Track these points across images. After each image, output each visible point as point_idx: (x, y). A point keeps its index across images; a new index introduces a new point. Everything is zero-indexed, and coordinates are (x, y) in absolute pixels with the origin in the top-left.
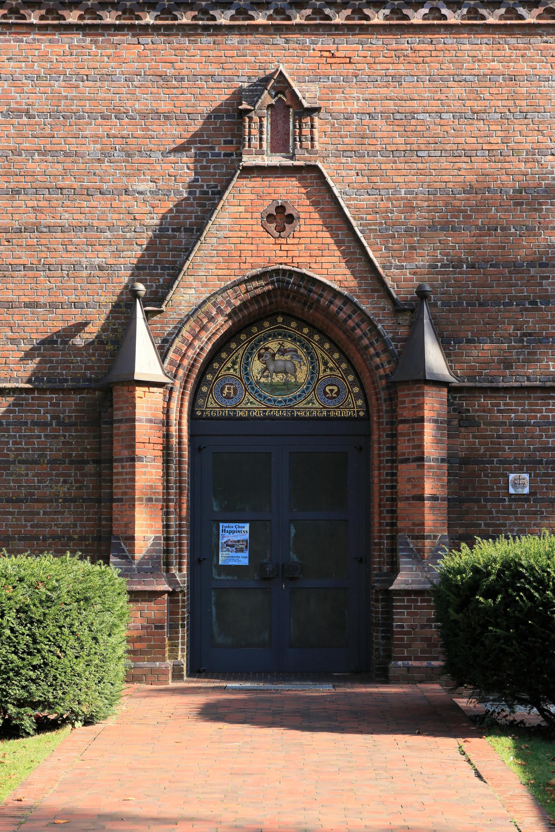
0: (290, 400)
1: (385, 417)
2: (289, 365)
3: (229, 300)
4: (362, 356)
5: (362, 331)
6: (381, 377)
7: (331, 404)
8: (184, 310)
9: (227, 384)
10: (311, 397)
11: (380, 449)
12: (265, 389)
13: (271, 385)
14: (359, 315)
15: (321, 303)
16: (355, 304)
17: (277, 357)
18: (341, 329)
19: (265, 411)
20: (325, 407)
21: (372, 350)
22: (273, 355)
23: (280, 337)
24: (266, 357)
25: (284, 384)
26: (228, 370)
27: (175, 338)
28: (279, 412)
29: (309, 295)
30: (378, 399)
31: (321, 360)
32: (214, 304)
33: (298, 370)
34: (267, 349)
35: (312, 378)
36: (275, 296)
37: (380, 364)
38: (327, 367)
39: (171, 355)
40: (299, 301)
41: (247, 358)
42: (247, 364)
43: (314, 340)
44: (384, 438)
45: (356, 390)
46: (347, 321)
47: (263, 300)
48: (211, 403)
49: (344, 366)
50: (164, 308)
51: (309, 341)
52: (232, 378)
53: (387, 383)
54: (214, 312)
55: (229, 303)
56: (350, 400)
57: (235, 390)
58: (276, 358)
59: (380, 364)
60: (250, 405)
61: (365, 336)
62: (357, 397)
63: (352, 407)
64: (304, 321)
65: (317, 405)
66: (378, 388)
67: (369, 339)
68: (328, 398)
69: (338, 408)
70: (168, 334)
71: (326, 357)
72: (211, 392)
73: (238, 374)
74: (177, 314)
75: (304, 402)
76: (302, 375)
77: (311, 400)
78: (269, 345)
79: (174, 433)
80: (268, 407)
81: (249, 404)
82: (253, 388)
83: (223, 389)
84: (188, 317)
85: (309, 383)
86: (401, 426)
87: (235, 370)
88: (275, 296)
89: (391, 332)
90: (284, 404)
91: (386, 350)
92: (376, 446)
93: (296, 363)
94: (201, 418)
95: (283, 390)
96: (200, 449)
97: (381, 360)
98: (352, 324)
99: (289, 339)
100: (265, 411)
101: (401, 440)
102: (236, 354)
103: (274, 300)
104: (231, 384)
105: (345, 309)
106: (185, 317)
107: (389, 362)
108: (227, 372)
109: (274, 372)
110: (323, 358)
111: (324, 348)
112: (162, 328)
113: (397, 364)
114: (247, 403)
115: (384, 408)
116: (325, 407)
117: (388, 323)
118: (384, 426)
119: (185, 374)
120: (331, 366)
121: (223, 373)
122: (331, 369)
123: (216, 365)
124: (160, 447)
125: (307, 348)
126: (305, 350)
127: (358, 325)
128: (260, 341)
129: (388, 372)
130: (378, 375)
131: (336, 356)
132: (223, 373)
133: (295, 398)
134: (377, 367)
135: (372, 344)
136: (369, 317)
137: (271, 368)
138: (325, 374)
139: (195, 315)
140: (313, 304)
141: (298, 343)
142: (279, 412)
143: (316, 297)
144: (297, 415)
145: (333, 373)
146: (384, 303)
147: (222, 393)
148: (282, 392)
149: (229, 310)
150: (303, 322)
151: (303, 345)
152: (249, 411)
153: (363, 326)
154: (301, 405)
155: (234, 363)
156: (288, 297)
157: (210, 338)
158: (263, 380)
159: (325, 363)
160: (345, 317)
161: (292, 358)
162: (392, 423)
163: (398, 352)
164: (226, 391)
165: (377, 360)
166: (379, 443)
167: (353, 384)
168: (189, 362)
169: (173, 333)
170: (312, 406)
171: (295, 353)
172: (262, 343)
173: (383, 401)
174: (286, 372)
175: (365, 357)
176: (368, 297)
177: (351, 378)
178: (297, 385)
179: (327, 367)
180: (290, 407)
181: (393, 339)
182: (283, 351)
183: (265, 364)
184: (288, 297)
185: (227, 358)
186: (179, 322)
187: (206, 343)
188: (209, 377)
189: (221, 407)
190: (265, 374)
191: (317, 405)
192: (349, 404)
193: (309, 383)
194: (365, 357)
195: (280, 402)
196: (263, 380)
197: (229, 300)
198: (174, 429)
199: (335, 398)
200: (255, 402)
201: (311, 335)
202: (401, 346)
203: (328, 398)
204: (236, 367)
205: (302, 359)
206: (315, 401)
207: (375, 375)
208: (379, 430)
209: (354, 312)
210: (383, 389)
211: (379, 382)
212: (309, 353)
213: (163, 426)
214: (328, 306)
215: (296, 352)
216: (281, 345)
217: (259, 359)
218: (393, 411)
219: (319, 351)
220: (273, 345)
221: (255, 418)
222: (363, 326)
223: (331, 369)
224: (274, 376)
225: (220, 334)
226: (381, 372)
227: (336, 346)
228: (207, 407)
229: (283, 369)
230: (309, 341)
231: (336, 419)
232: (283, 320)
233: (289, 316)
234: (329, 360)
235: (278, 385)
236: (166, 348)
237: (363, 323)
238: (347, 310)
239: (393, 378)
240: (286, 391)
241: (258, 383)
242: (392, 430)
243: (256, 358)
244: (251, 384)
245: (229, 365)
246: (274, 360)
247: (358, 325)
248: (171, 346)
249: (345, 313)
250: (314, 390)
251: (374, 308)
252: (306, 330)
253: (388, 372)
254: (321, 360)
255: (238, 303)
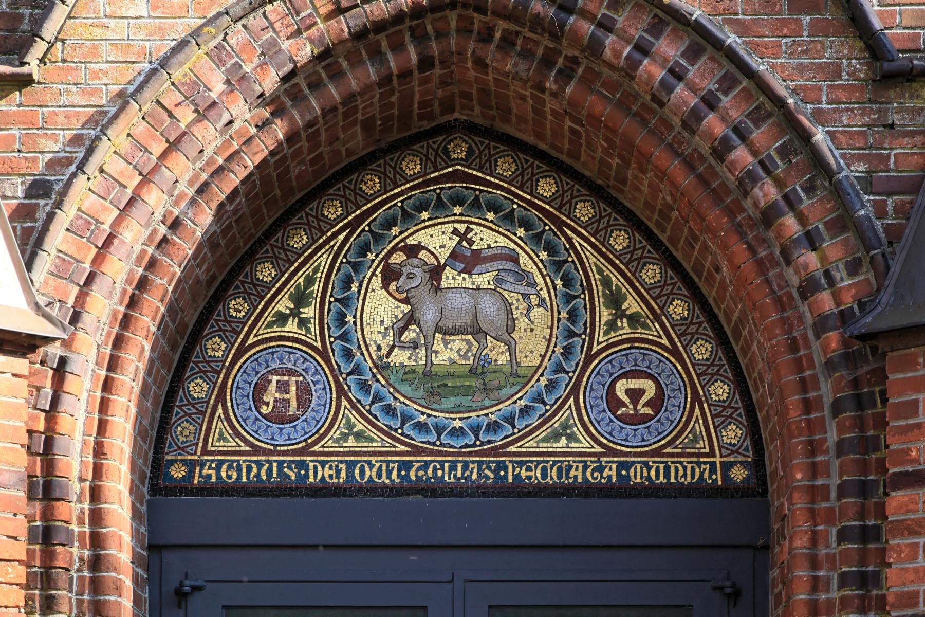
0: (494, 427)
1: (835, 471)
2: (489, 307)
3: (273, 43)
4: (752, 249)
5: (754, 153)
6: (821, 325)
7: (632, 439)
8: (111, 80)
9: (275, 372)
10: (563, 415)
11: (815, 585)
12: (405, 389)
13: (428, 374)
14: (747, 95)
15: (608, 52)
16: (731, 55)
17: (449, 278)
18: (678, 154)
19: (407, 466)
20: (611, 452)
21: (790, 224)
22: (436, 272)
23: (457, 210)
24: (410, 277)
25: (472, 371)
26: (282, 316)
27: (74, 175)
28: (453, 467)
29: (562, 25)
30: (808, 406)
31: (598, 289)
32: (218, 55)
33: (522, 323)
34: (413, 251)
35: (567, 352)
36: (441, 35)
37: (819, 274)
38: (621, 314)
39: (58, 238)
40: (527, 54)
41: (347, 283)
42: (345, 302)
43: (576, 220)
44: (831, 546)
45: (720, 391)
46: (700, 119)
47: (398, 47)
48: (221, 437)
49: (678, 309)
50: (32, 67)
51: (560, 224)
52: (291, 351)
53: (845, 343)
54: (218, 87)
55: (270, 52)
56: (700, 427)
57: (304, 392)
58: (444, 284)
59: (819, 274)
60: (351, 445)
61: (768, 172)
62: (722, 415)
63: (711, 447)
64: (542, 156)
65: (584, 444)
66: (812, 366)
67: (779, 183)
68: (624, 419)
69: (657, 453)
70: (50, 165)
71: (616, 280)
72: (221, 398)
73: (313, 336)
74: (84, 92)
75: (542, 433)
76: (534, 337)
77: (565, 426)
78: (422, 237)
79: (75, 527)
80: (417, 451)
81: (351, 441)
82: (364, 386)
83: (260, 389)
84: (123, 99)
85: (559, 369)
86: (899, 497)
87: (303, 323)
88: (441, 35)
89: (860, 158)
90: (470, 439)
91: (844, 221)
92: (802, 573)
93: (512, 297)
94: (184, 488)
95: (468, 391)
96: (181, 596)
97: (823, 259)
98: (720, 129)
99: (490, 216)
100: (407, 466)
101: (898, 549)
102: (307, 270)
103: (435, 48)
104: (291, 373)
105: (693, 72)
106: (111, 101)
107: (853, 268)
108: (276, 331)
109: (438, 329)
110: (606, 282)
111: (611, 249)
112: (29, 145)
113: (883, 273)
114: (345, 437)
115: (832, 436)
116: (611, 452)
117: (853, 122)
118: (832, 502)
119: (114, 314)
120: (632, 304)
121: (262, 332)
122: (634, 320)
123: (237, 307)
124: (18, 573)
125: (551, 249)
126: (544, 255)
127: (741, 133)
128: (389, 224)
129: (848, 301)
130: (809, 319)
131: (651, 273)
132: (262, 332)
133: (510, 420)
134: (809, 288)
135: (790, 201)
136: (780, 103)
137: (429, 315)
138: (614, 337)
139: (148, 94)
140: (574, 61)
141: (521, 232)
142: (453, 467)
143: (588, 28)
144: (517, 477)
145: (641, 333)
146: (839, 51)
147: (258, 401)
148: (466, 401)
149: (270, 81)
150: (538, 158)
151: (537, 238)
152: (351, 466)
153: (758, 135)
154: (530, 444)
155: (300, 299)
156: (486, 37)
157: (206, 184)
158: (400, 357)
159: (615, 301)
160: (694, 101)
161: (498, 280)
162: (864, 489)
163: (887, 228)
164: (271, 395)
165: (811, 259)
166: (814, 564)
167: (708, 371)
168: (131, 273)
169: (69, 162)
170: (569, 445)
171: (510, 265)
172: (395, 231)
173: (827, 412)
174: (477, 331)
175: (762, 253)
176: (779, 29)
177: (702, 350)
178: (517, 376)
179: (621, 314)
180: (494, 452)
181: (868, 182)
182: (467, 259)
183: (406, 301)
184: (486, 37)
185: (276, 280)
186: (92, 122)
187: (193, 202)
188: (216, 347)
189: (256, 450)
190: (409, 335)
191: (584, 444)
192: (695, 440)
193: (559, 369)
194: (762, 253)
195: (458, 433)
196: (400, 357)
197: (273, 43)
198: (73, 511)
199: (646, 418)
200: (372, 433)
201: (563, 201)
202: (899, 210)
203: (624, 419)
204: (308, 312)
205: (533, 285)
206: (578, 430)
207: (801, 318)
208: (813, 515)
209: (727, 83)
210: (830, 366)
211: (816, 345)
212: (558, 265)
213: (31, 498)
214: (633, 64)
215: (516, 261)
216: (463, 237)
217: (385, 286)
218: (866, 444)
219: (592, 259)
220: (437, 239)
221: (372, 490)
222: (758, 135)
223: (634, 320)
224: (438, 345)
225: (243, 173)
226: (825, 301)
227: (651, 240)
228: (205, 452)
229: (468, 319)
230: (560, 224)
231: (651, 491)
232: (470, 152)
233: (492, 137)
234: (625, 288)
235: (451, 375)
236: (41, 216)
237: (757, 123)
238: (703, 75)
239: (868, 323)
240: (479, 396)
241: (382, 367)
242: (862, 514)
243: (377, 282)
244: (357, 370)
245: (284, 304)
246: (438, 289)
247: (741, 133)
248: (59, 205)
249: (693, 89)
250: (575, 391)
251: (801, 68)
252: (547, 188)
253: (848, 301)
254: (598, 289)
255: (304, 51)
